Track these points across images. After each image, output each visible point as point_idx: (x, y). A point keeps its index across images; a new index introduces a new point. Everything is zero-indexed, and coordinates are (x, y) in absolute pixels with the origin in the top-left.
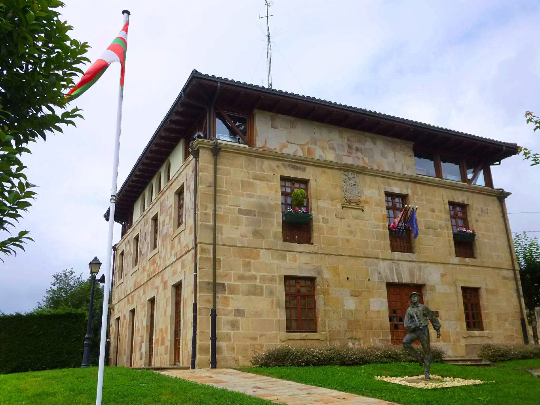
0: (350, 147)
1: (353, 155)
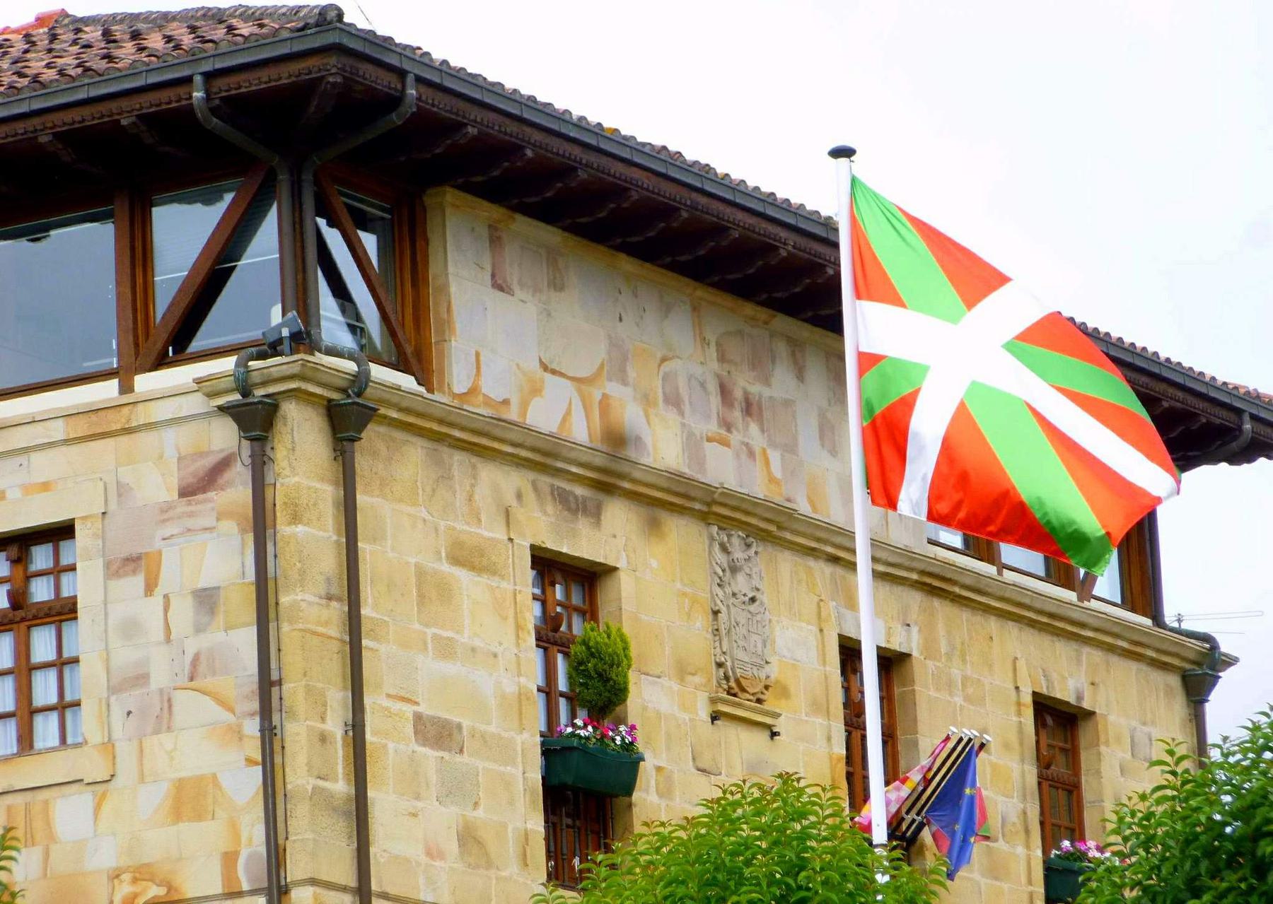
0: (725, 392)
1: (735, 438)
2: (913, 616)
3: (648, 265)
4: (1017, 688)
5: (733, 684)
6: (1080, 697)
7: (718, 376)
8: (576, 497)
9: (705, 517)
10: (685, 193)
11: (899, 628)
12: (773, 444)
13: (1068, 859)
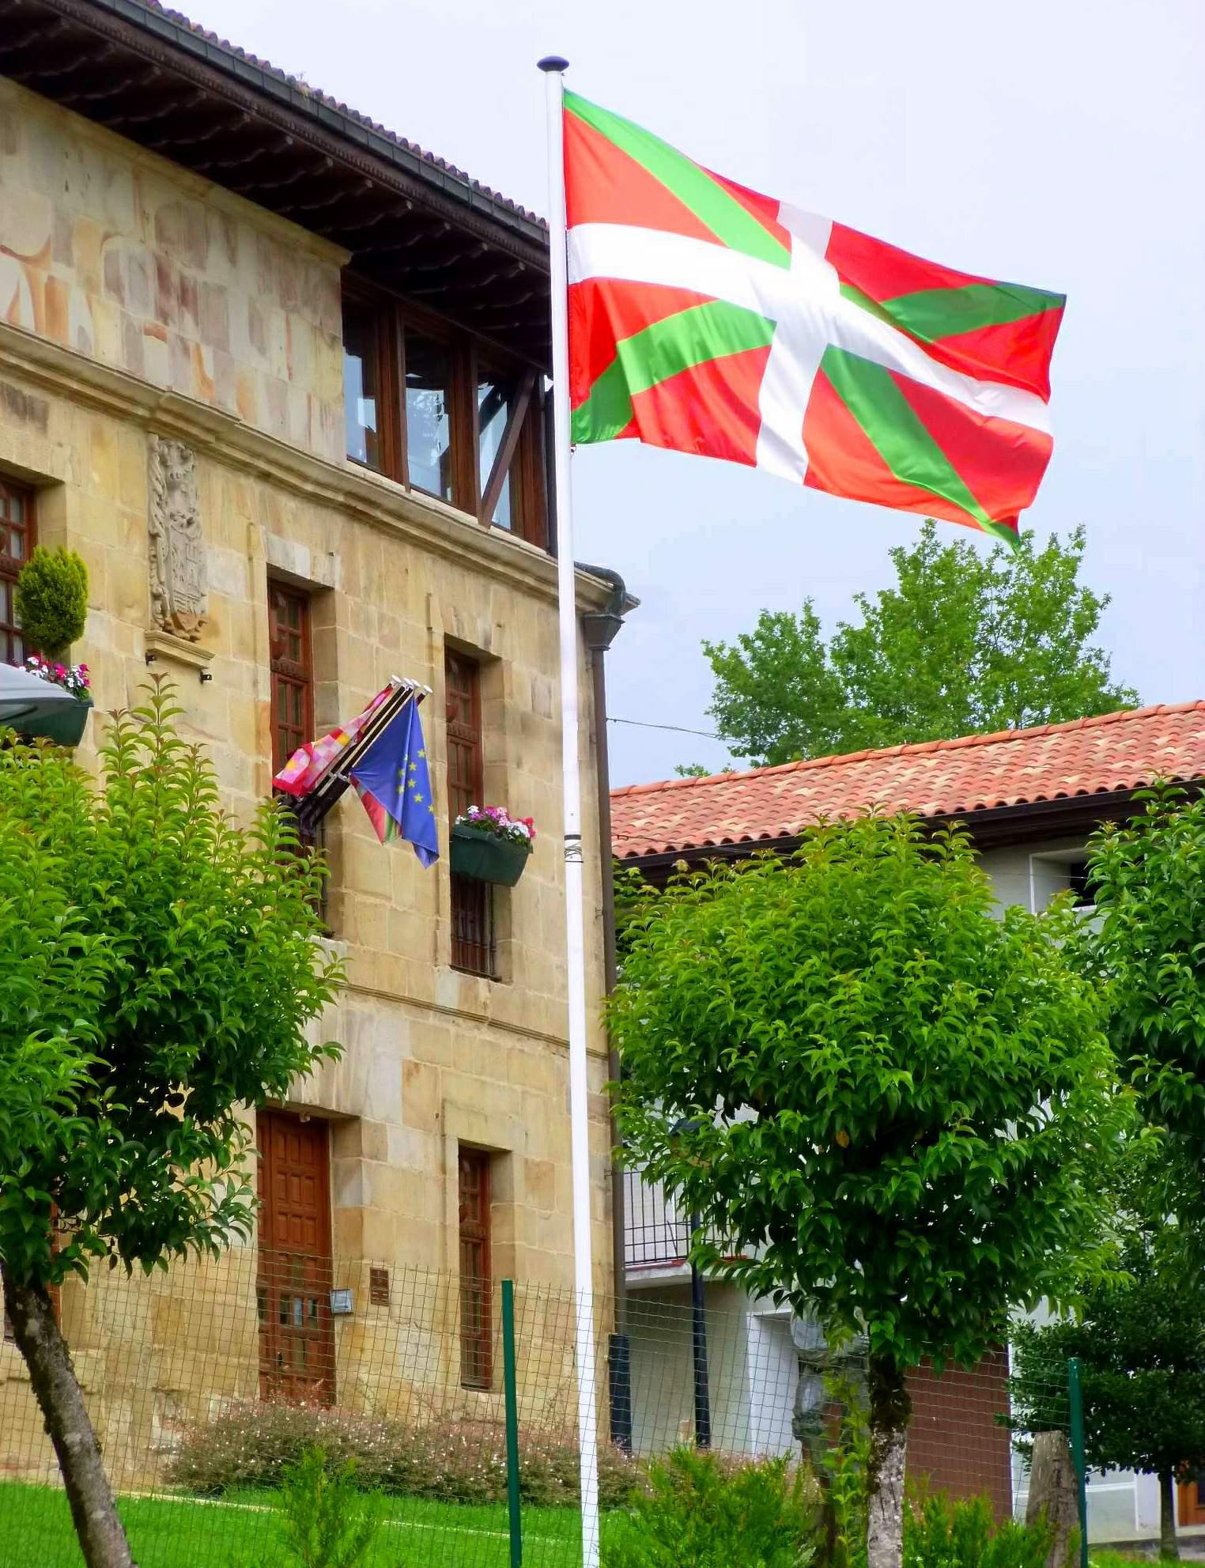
0: (162, 275)
1: (171, 330)
2: (336, 544)
3: (96, 125)
4: (429, 629)
5: (169, 619)
6: (487, 642)
7: (157, 258)
8: (24, 398)
9: (146, 425)
10: (158, 46)
11: (323, 558)
12: (207, 340)
13: (477, 827)
